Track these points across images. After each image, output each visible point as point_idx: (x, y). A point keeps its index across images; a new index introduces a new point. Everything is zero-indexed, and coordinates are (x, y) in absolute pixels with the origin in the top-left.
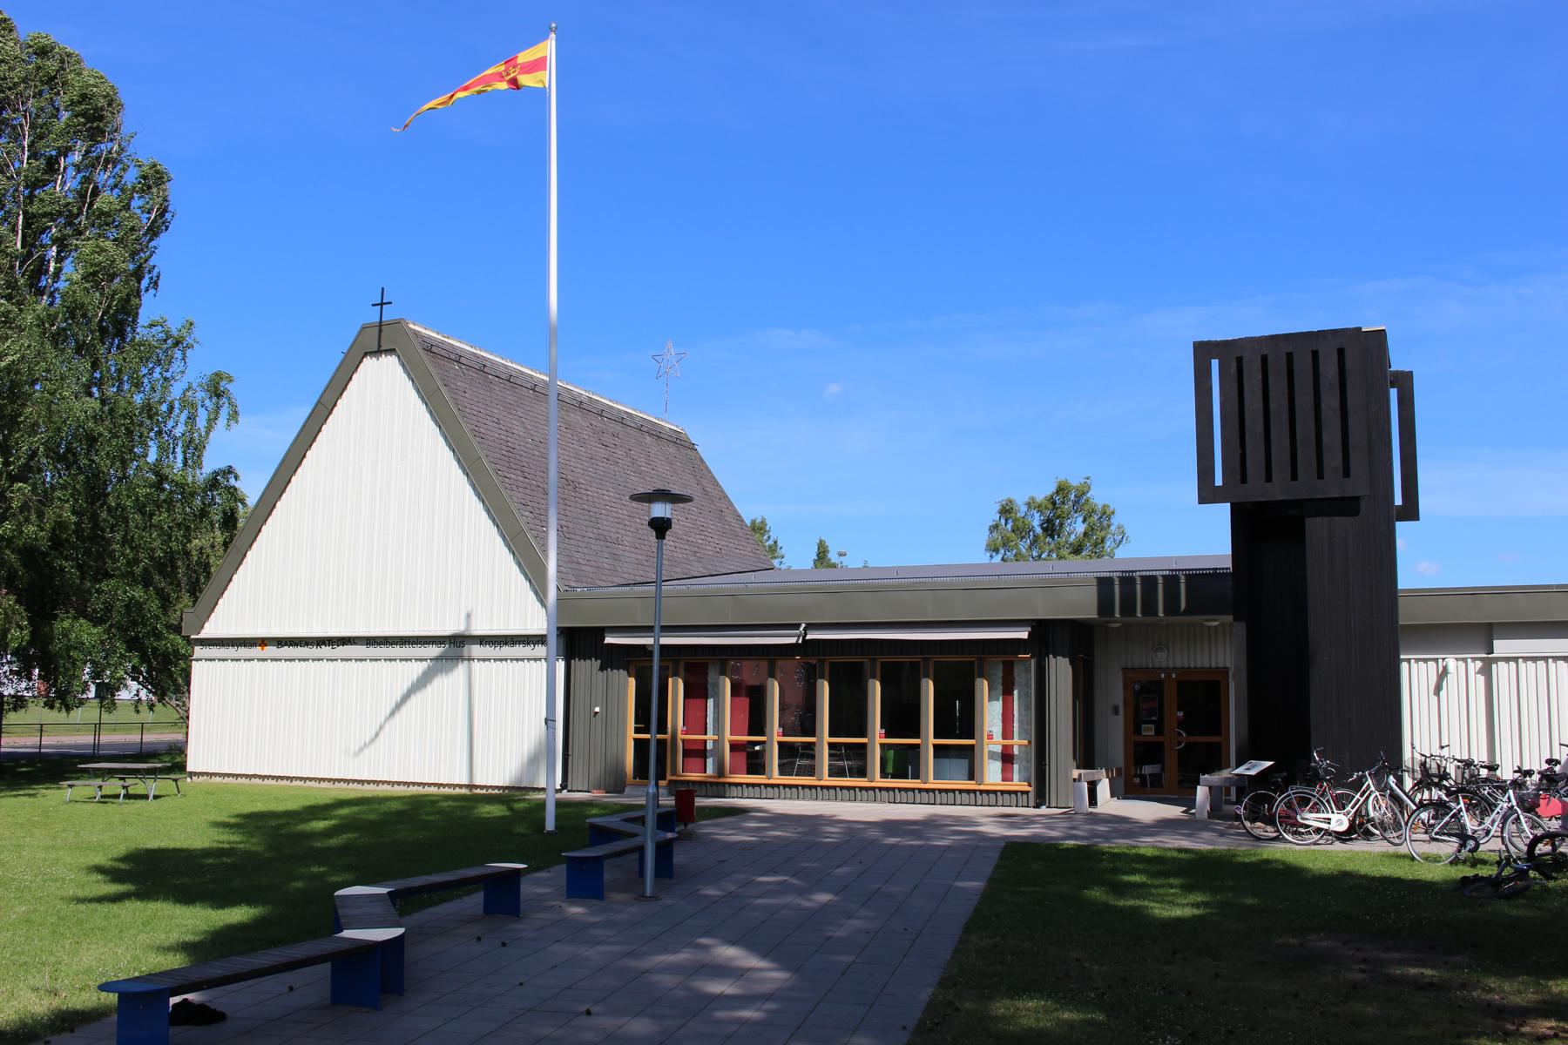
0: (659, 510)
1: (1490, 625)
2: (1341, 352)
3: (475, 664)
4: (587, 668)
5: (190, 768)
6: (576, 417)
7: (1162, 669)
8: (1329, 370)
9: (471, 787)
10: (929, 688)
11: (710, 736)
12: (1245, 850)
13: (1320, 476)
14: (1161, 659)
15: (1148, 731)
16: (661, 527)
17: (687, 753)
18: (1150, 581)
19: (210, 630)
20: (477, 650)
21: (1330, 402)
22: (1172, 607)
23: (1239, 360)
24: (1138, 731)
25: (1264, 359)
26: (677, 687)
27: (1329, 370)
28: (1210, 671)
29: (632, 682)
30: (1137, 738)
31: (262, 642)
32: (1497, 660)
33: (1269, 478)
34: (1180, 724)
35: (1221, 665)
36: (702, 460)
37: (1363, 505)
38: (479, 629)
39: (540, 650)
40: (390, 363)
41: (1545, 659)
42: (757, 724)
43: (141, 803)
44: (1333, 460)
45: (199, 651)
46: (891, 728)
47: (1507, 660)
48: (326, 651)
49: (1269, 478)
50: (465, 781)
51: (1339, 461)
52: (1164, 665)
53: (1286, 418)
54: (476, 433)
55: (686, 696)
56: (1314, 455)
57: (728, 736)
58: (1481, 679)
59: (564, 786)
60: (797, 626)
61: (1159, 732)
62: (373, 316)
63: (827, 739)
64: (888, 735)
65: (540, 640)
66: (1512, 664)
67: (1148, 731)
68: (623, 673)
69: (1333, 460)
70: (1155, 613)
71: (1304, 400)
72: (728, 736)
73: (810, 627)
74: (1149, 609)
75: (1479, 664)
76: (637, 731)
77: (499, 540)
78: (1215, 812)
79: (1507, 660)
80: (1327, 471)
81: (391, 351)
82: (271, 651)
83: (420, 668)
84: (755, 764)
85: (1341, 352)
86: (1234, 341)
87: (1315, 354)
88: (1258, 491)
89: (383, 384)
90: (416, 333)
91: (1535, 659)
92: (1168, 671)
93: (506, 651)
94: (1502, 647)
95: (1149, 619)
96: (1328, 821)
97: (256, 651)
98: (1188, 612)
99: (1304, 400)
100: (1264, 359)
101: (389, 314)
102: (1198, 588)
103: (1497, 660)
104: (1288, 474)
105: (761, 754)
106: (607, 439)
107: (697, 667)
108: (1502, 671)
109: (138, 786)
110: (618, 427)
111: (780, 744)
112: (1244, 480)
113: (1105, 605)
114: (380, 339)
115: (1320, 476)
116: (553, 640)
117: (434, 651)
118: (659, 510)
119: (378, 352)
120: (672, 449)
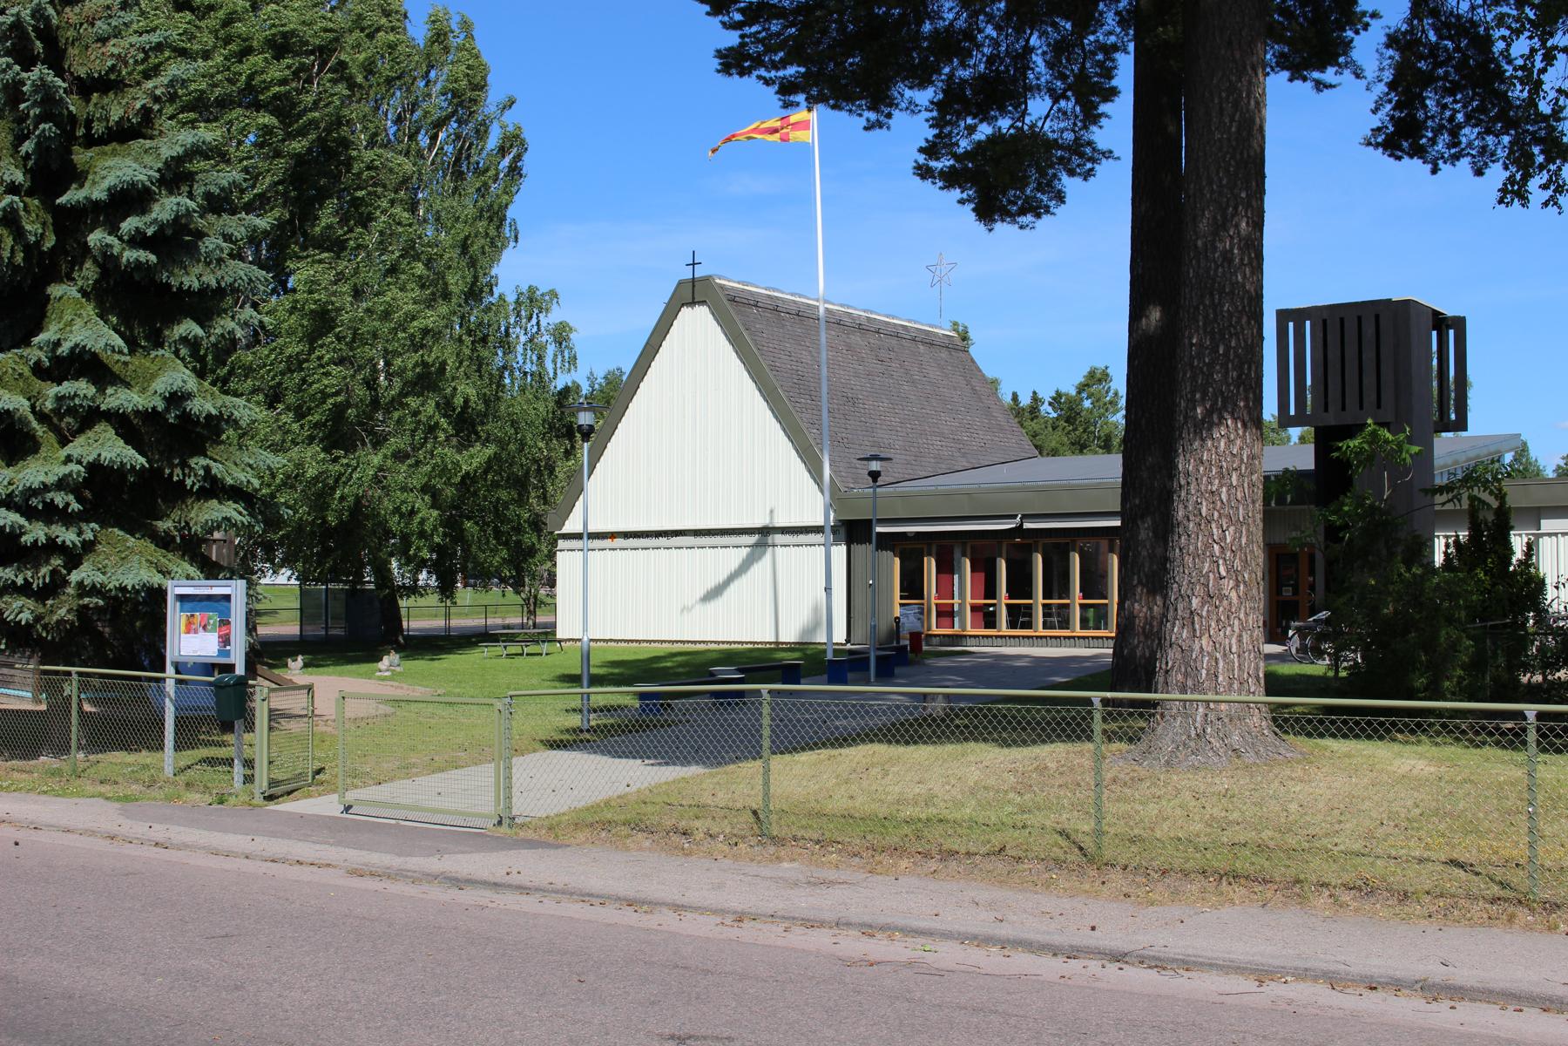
0: (875, 466)
2: (1377, 317)
3: (779, 550)
4: (864, 551)
5: (559, 636)
6: (856, 339)
8: (1369, 330)
9: (777, 643)
10: (1039, 561)
11: (956, 601)
15: (1287, 592)
16: (875, 475)
17: (939, 615)
19: (572, 525)
20: (779, 538)
24: (1279, 592)
26: (930, 565)
27: (1369, 330)
29: (897, 561)
31: (612, 535)
33: (1326, 410)
36: (973, 361)
38: (781, 522)
39: (819, 538)
40: (702, 312)
42: (991, 592)
43: (537, 658)
44: (1370, 397)
45: (561, 544)
46: (1086, 593)
47: (1550, 535)
48: (662, 541)
50: (773, 640)
51: (1374, 397)
53: (1338, 366)
54: (773, 368)
55: (938, 572)
57: (969, 600)
59: (848, 641)
60: (1015, 517)
61: (1295, 592)
62: (687, 274)
63: (1041, 600)
64: (1084, 598)
65: (817, 530)
68: (890, 553)
71: (1351, 351)
72: (969, 600)
73: (1024, 517)
76: (902, 598)
77: (793, 452)
78: (1302, 649)
79: (1550, 535)
80: (1365, 404)
81: (703, 303)
82: (619, 542)
83: (745, 552)
84: (990, 620)
85: (1377, 317)
89: (697, 323)
90: (722, 287)
93: (802, 538)
97: (607, 543)
98: (1292, 503)
99: (1351, 351)
101: (700, 272)
105: (994, 614)
106: (883, 354)
107: (946, 549)
109: (533, 648)
110: (894, 341)
111: (1008, 606)
114: (693, 292)
116: (828, 530)
117: (753, 539)
118: (875, 466)
119: (692, 303)
120: (944, 354)
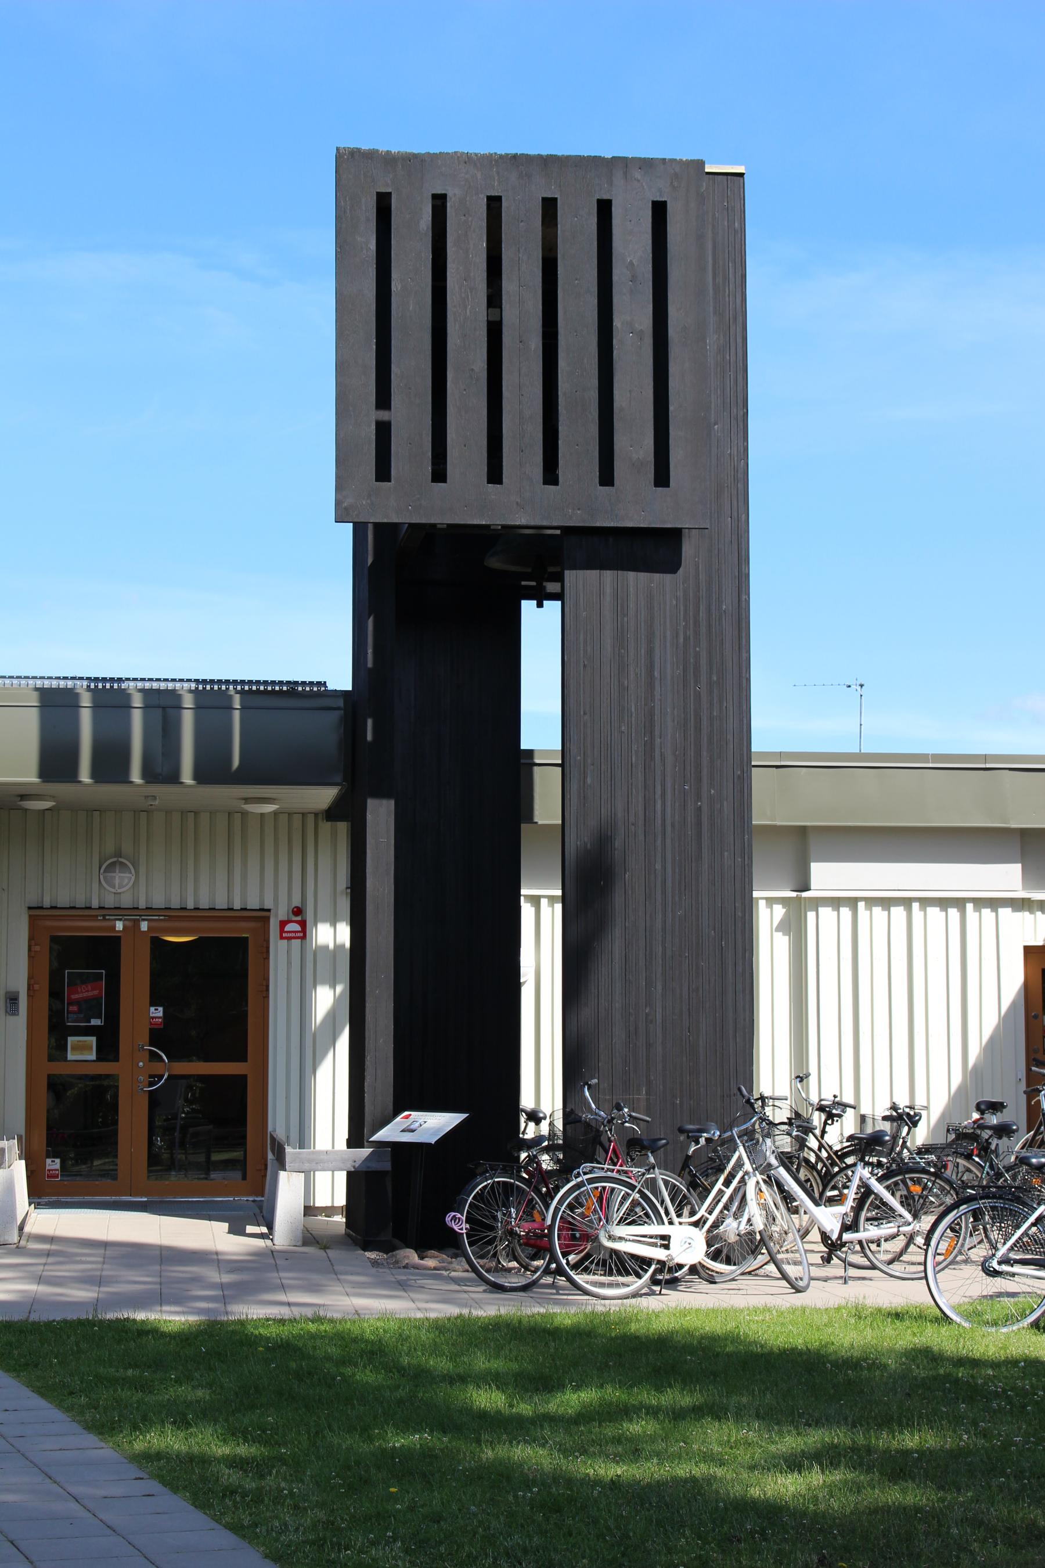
1: (802, 832)
2: (659, 210)
7: (119, 911)
12: (531, 1309)
13: (607, 478)
14: (123, 888)
18: (162, 702)
21: (633, 314)
22: (213, 769)
23: (439, 202)
24: (58, 1050)
25: (494, 203)
28: (228, 915)
30: (59, 1069)
32: (817, 903)
33: (495, 475)
34: (157, 1037)
35: (253, 903)
37: (688, 549)
41: (906, 903)
44: (634, 444)
47: (836, 903)
49: (495, 475)
52: (126, 901)
53: (535, 343)
56: (594, 429)
58: (783, 942)
61: (108, 1049)
66: (954, 913)
67: (82, 1051)
69: (634, 444)
70: (174, 778)
74: (162, 770)
75: (779, 911)
79: (836, 903)
86: (434, 157)
87: (604, 208)
88: (410, 501)
91: (887, 903)
92: (133, 913)
94: (828, 876)
95: (110, 791)
96: (665, 1241)
100: (494, 203)
102: (257, 731)
103: (817, 903)
104: (537, 471)
108: (826, 926)
112: (383, 473)
113: (57, 761)
115: (607, 478)
